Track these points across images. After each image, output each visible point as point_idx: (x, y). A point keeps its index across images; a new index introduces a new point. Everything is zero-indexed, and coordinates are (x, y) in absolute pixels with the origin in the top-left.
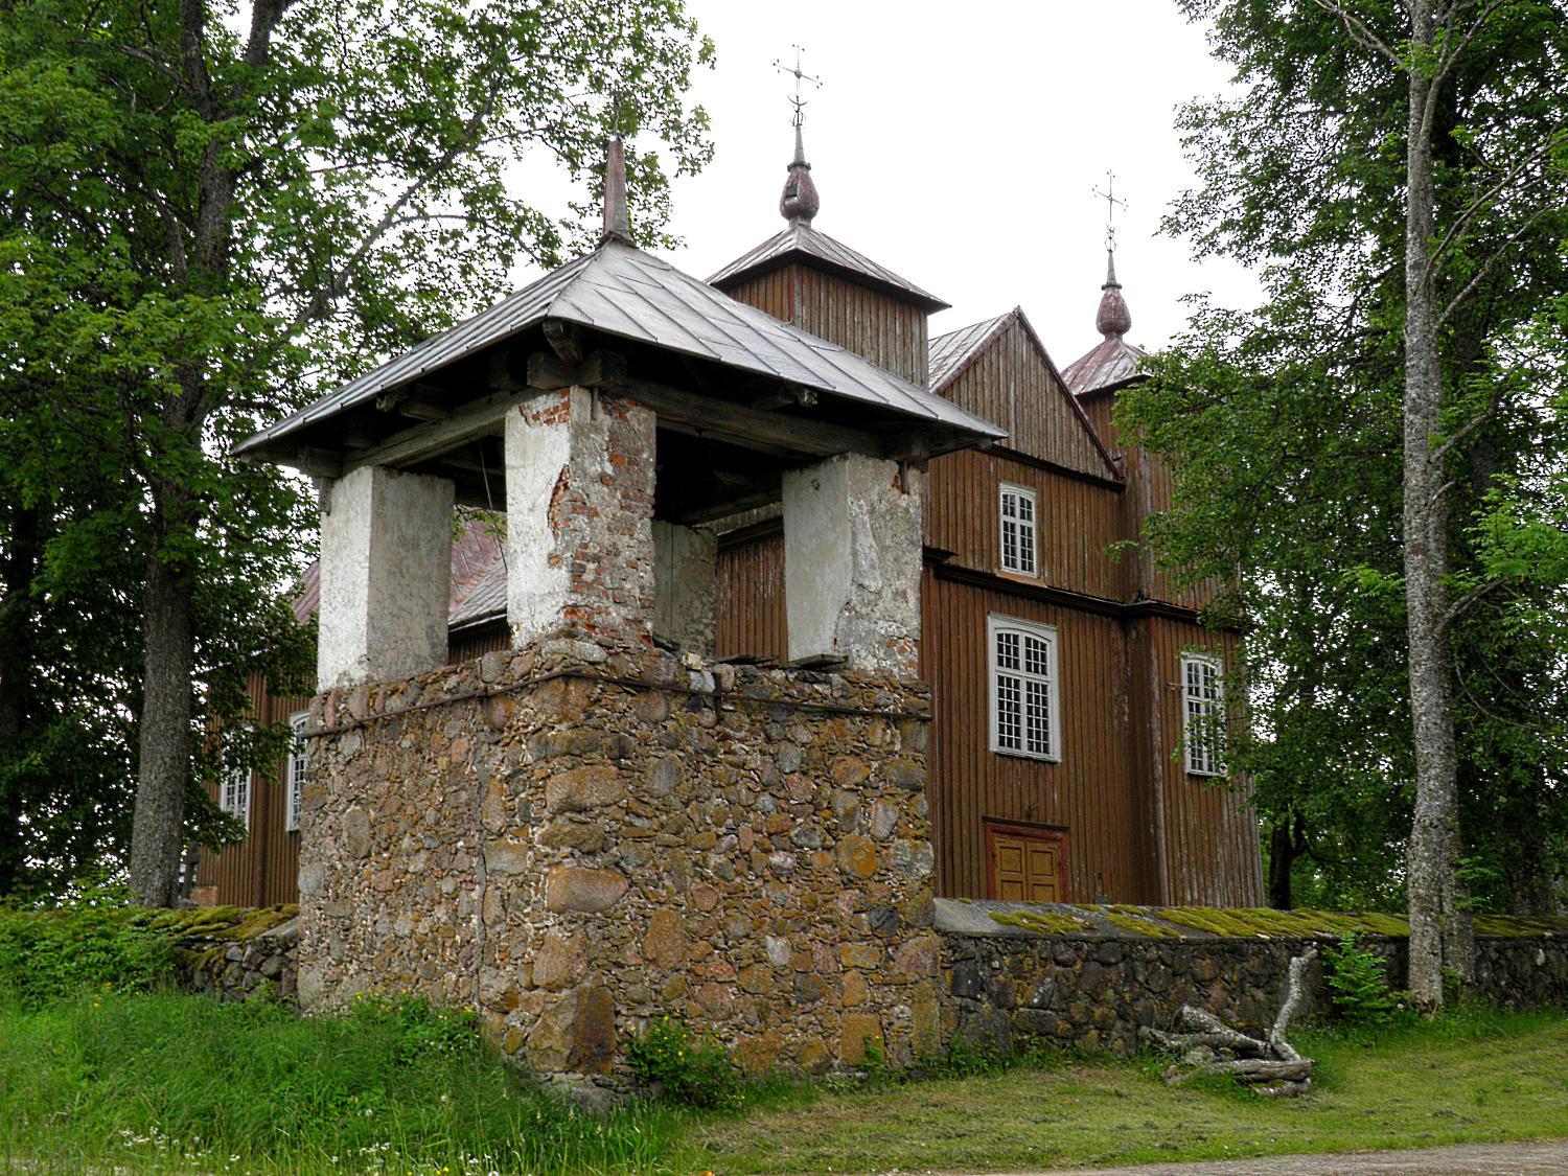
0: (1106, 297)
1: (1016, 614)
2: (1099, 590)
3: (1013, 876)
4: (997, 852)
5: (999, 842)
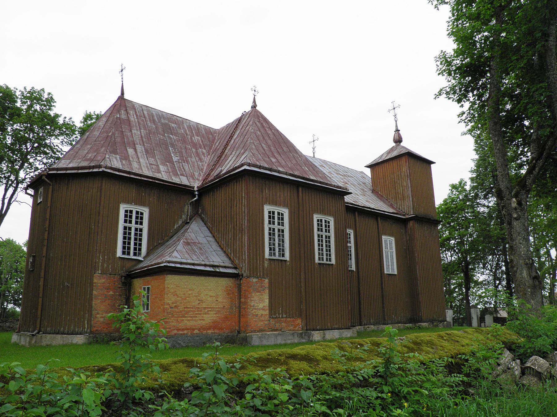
1: (382, 240)
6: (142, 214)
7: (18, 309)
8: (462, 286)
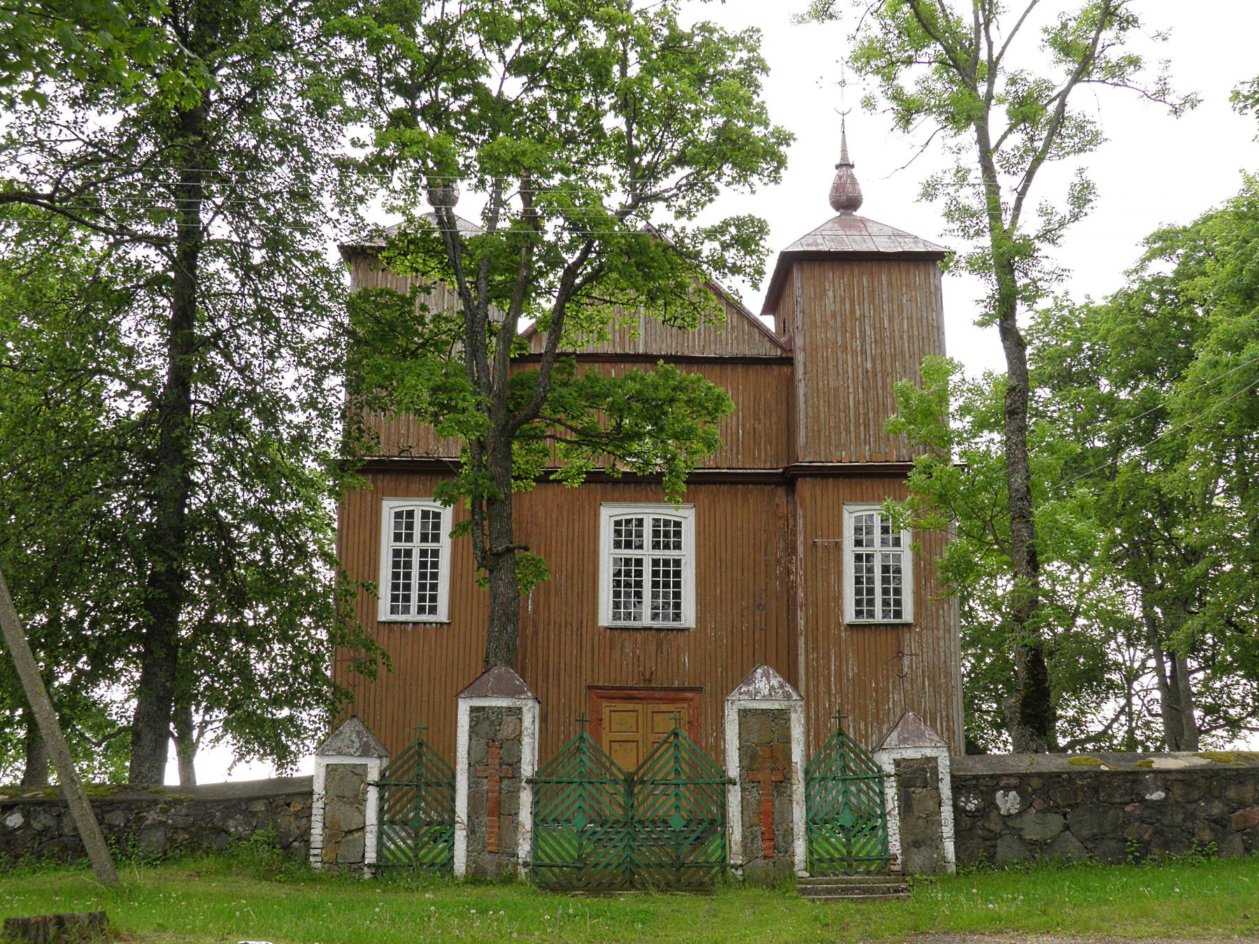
2: (764, 463)
3: (625, 736)
4: (605, 716)
5: (606, 708)
6: (678, 524)
8: (1092, 659)
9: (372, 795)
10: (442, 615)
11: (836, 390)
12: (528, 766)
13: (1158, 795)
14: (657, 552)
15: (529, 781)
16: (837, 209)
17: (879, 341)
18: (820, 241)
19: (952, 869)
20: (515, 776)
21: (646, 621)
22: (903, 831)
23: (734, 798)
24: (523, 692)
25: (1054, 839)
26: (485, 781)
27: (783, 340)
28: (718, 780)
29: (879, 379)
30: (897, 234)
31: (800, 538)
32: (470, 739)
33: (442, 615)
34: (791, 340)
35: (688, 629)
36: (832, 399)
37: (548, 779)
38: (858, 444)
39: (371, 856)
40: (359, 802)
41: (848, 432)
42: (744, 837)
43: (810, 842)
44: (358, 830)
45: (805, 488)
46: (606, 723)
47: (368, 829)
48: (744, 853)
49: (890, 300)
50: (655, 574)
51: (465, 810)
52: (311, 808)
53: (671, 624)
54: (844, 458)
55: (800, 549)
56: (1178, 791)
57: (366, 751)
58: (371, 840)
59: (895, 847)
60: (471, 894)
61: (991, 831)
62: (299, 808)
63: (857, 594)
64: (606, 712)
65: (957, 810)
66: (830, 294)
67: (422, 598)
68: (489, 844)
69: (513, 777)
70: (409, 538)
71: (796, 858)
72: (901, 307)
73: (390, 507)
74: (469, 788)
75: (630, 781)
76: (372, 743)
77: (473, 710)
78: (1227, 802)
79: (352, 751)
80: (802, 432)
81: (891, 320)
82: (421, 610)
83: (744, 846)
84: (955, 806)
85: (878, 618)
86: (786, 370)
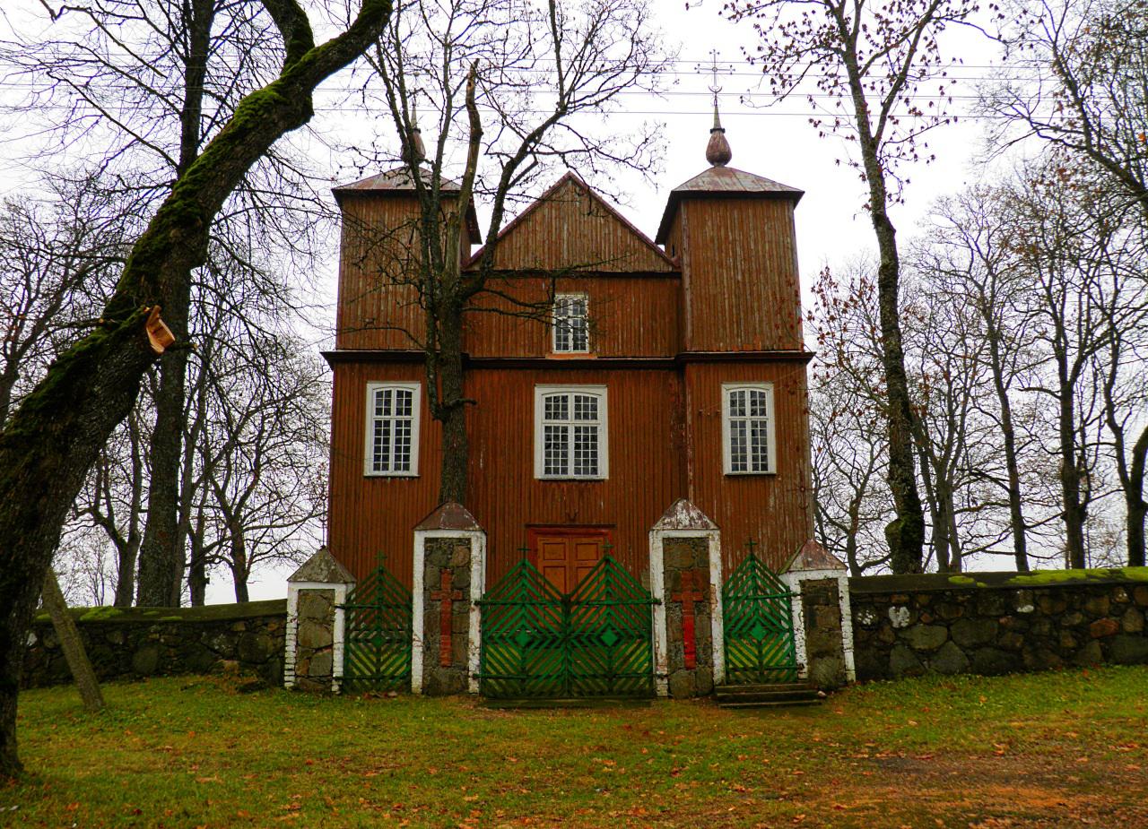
0: (713, 139)
1: (561, 382)
2: (660, 353)
3: (555, 563)
5: (540, 541)
6: (594, 400)
7: (133, 605)
9: (339, 616)
10: (414, 471)
11: (715, 296)
12: (476, 592)
13: (1028, 608)
14: (578, 421)
15: (477, 603)
16: (712, 162)
17: (747, 259)
18: (701, 184)
19: (852, 676)
20: (465, 599)
21: (571, 474)
22: (809, 643)
23: (660, 616)
24: (473, 525)
25: (940, 647)
26: (439, 603)
27: (673, 259)
28: (645, 601)
29: (748, 287)
30: (759, 179)
31: (689, 410)
32: (425, 566)
33: (414, 471)
34: (680, 259)
35: (603, 480)
36: (712, 303)
37: (494, 601)
38: (732, 338)
39: (338, 670)
40: (328, 622)
41: (724, 327)
42: (669, 651)
43: (726, 653)
44: (326, 647)
45: (692, 371)
46: (540, 553)
47: (335, 646)
48: (669, 665)
49: (755, 228)
50: (577, 438)
51: (421, 630)
52: (285, 628)
53: (590, 477)
54: (722, 348)
55: (689, 418)
56: (1045, 604)
57: (333, 579)
58: (338, 657)
59: (802, 657)
60: (427, 709)
61: (885, 642)
62: (276, 627)
63: (733, 452)
64: (540, 544)
65: (856, 625)
66: (709, 223)
67: (397, 458)
68: (443, 659)
69: (464, 600)
70: (388, 412)
71: (715, 669)
72: (763, 233)
73: (372, 388)
74: (425, 609)
75: (566, 603)
76: (340, 569)
77: (427, 540)
78: (1087, 613)
79: (321, 578)
80: (689, 328)
81: (756, 244)
82: (397, 468)
83: (669, 657)
84: (853, 621)
85: (750, 470)
86: (676, 282)
